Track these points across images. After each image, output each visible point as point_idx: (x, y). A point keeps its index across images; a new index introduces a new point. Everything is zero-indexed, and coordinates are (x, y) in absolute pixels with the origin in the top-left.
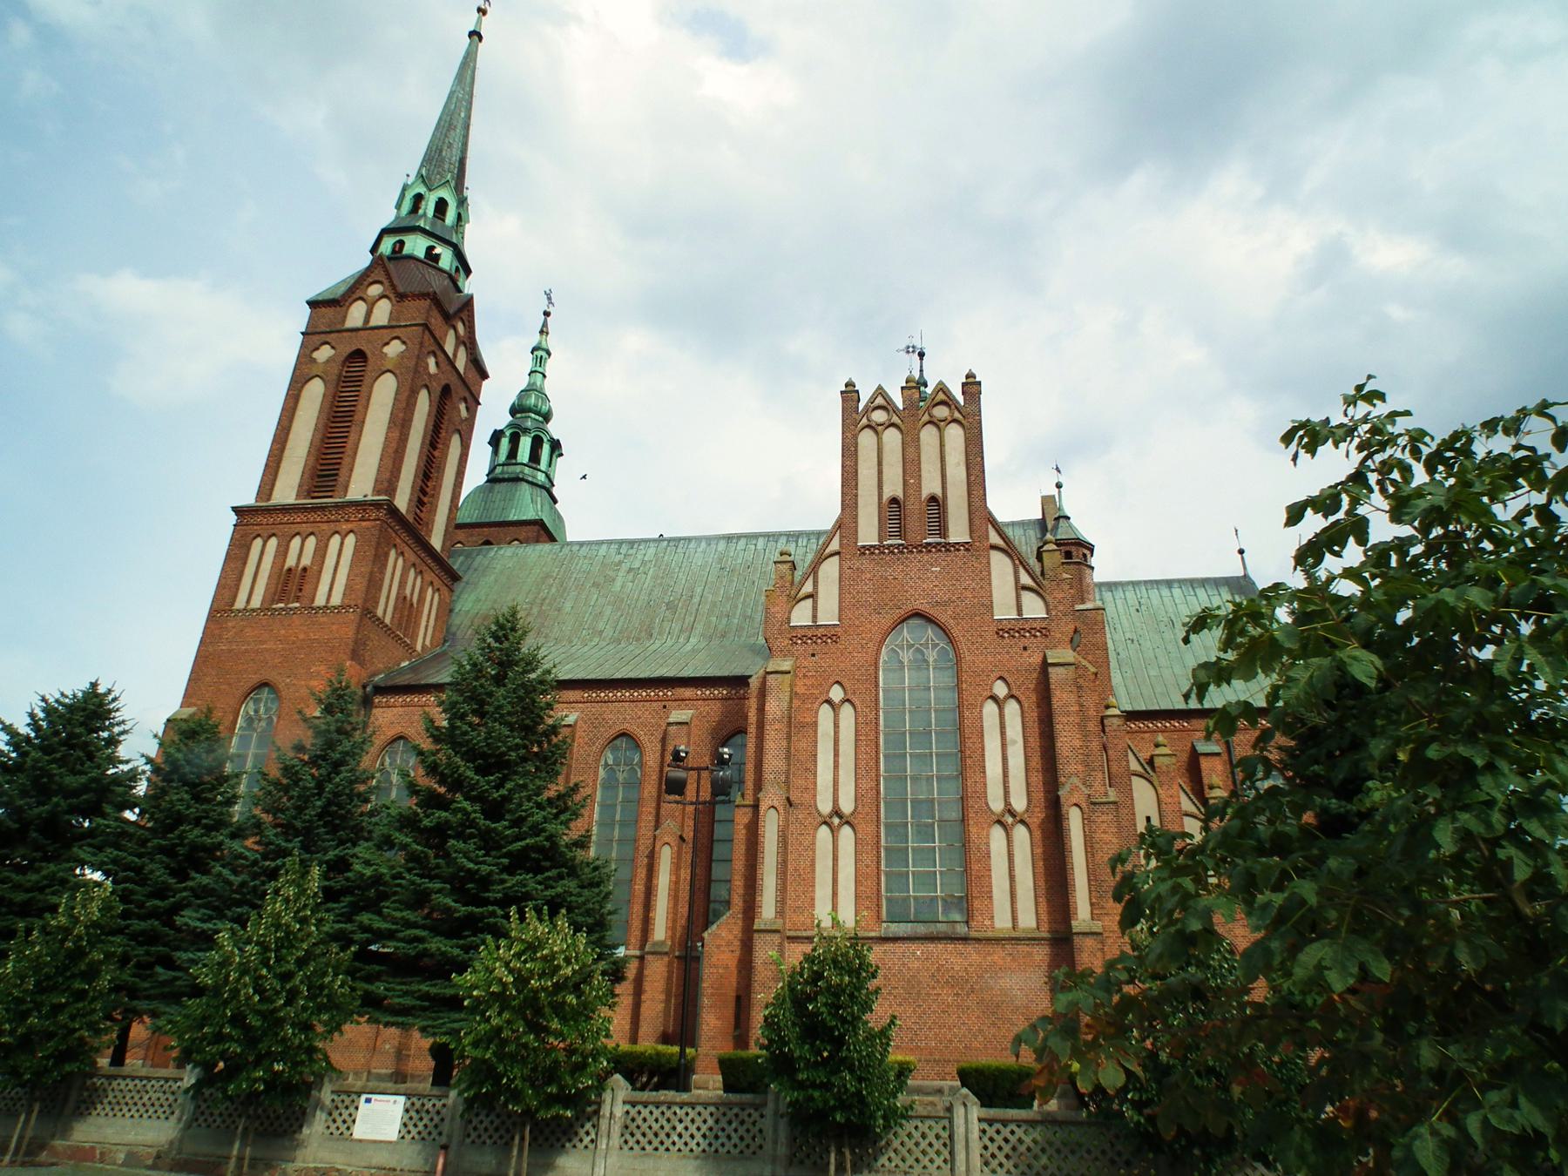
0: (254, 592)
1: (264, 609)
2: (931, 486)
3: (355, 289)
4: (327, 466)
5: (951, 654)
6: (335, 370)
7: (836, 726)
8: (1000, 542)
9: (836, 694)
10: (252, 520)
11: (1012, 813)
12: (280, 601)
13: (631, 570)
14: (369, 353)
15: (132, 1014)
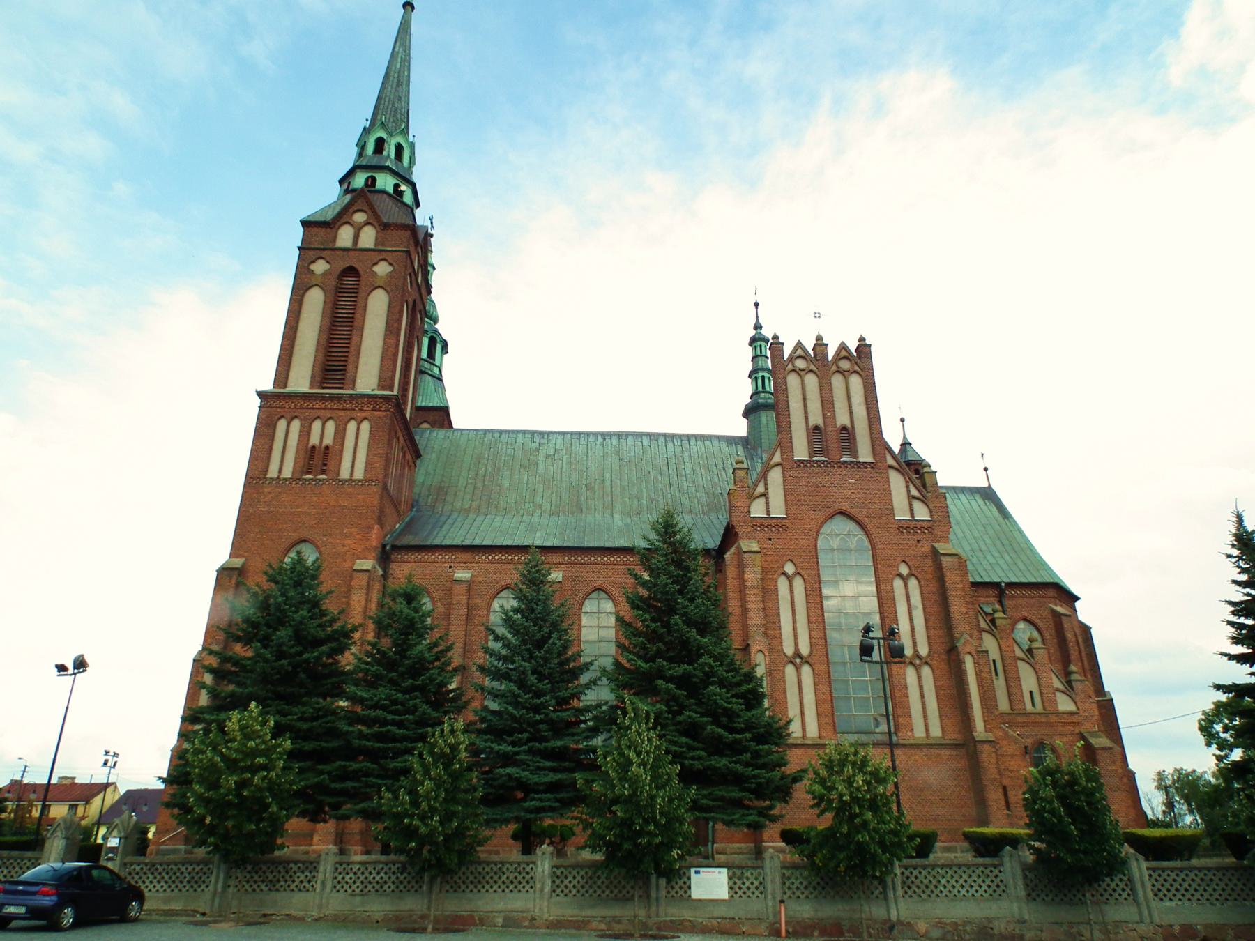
0: (284, 464)
1: (296, 478)
2: (842, 419)
3: (343, 216)
4: (335, 363)
5: (867, 543)
6: (332, 282)
7: (792, 592)
8: (895, 464)
9: (789, 568)
10: (275, 404)
11: (919, 657)
12: (307, 473)
13: (547, 456)
14: (361, 272)
15: (180, 809)
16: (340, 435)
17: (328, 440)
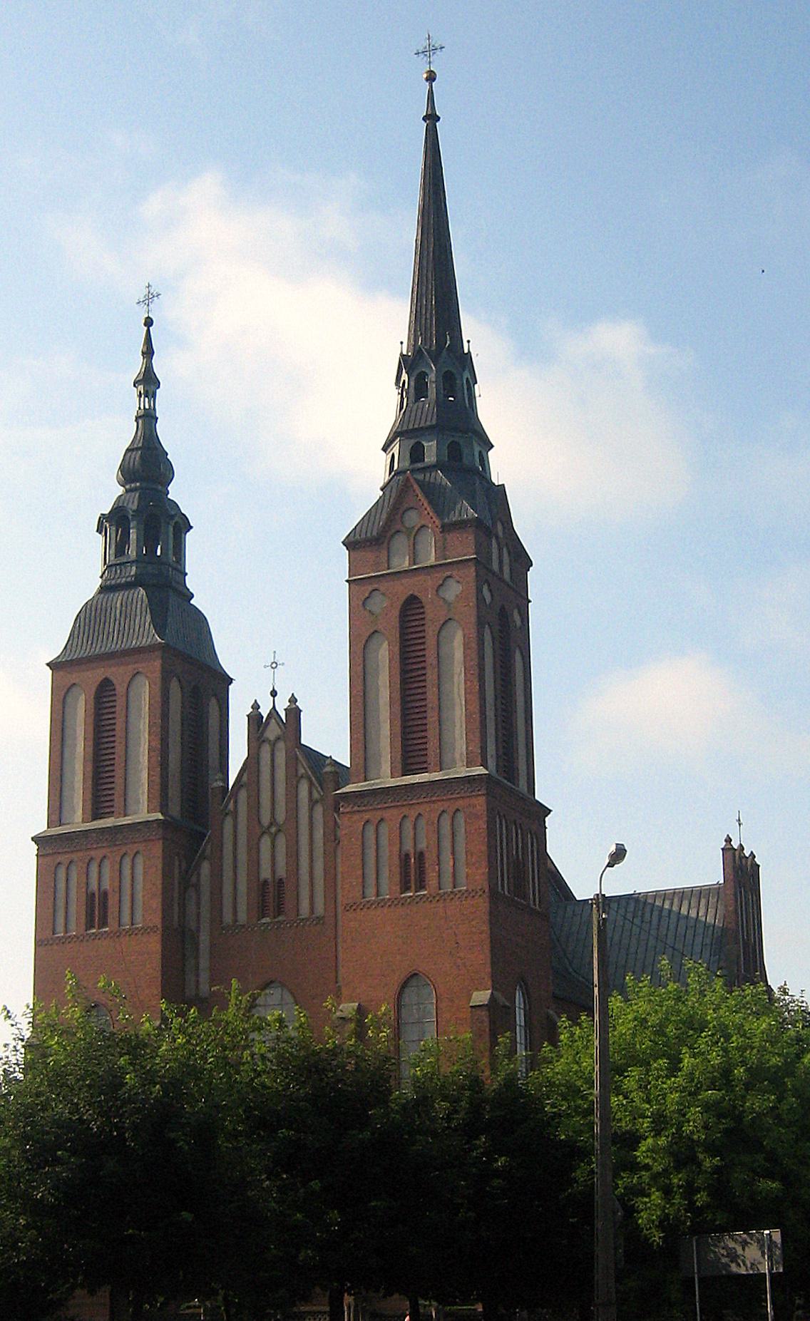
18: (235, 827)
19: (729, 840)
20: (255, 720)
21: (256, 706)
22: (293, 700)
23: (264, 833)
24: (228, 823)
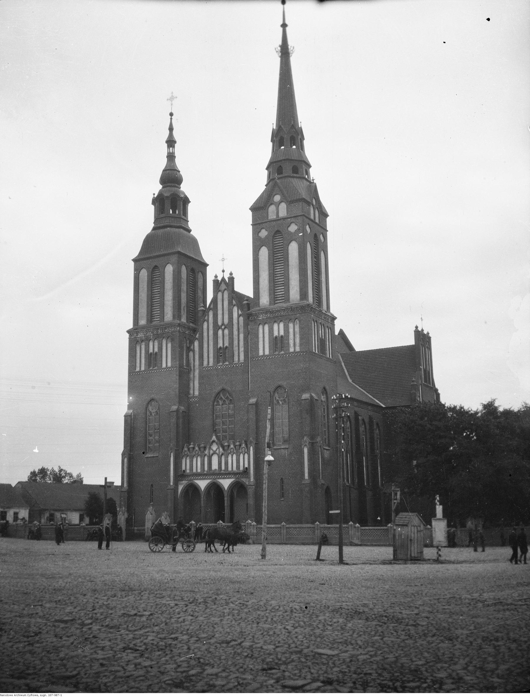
16: (160, 348)
17: (282, 333)
18: (208, 326)
19: (417, 327)
20: (217, 283)
21: (216, 277)
22: (231, 274)
23: (220, 328)
24: (205, 324)
